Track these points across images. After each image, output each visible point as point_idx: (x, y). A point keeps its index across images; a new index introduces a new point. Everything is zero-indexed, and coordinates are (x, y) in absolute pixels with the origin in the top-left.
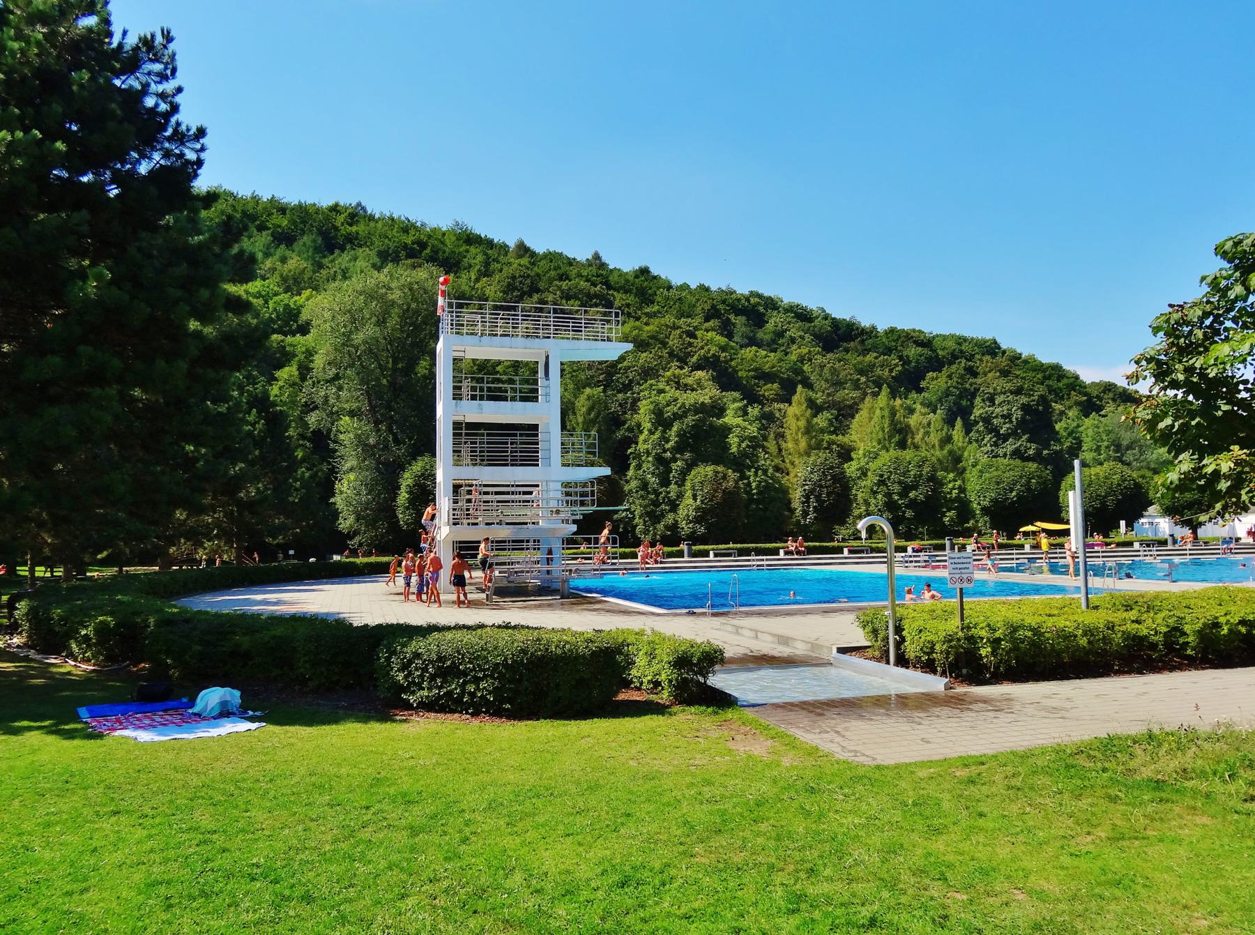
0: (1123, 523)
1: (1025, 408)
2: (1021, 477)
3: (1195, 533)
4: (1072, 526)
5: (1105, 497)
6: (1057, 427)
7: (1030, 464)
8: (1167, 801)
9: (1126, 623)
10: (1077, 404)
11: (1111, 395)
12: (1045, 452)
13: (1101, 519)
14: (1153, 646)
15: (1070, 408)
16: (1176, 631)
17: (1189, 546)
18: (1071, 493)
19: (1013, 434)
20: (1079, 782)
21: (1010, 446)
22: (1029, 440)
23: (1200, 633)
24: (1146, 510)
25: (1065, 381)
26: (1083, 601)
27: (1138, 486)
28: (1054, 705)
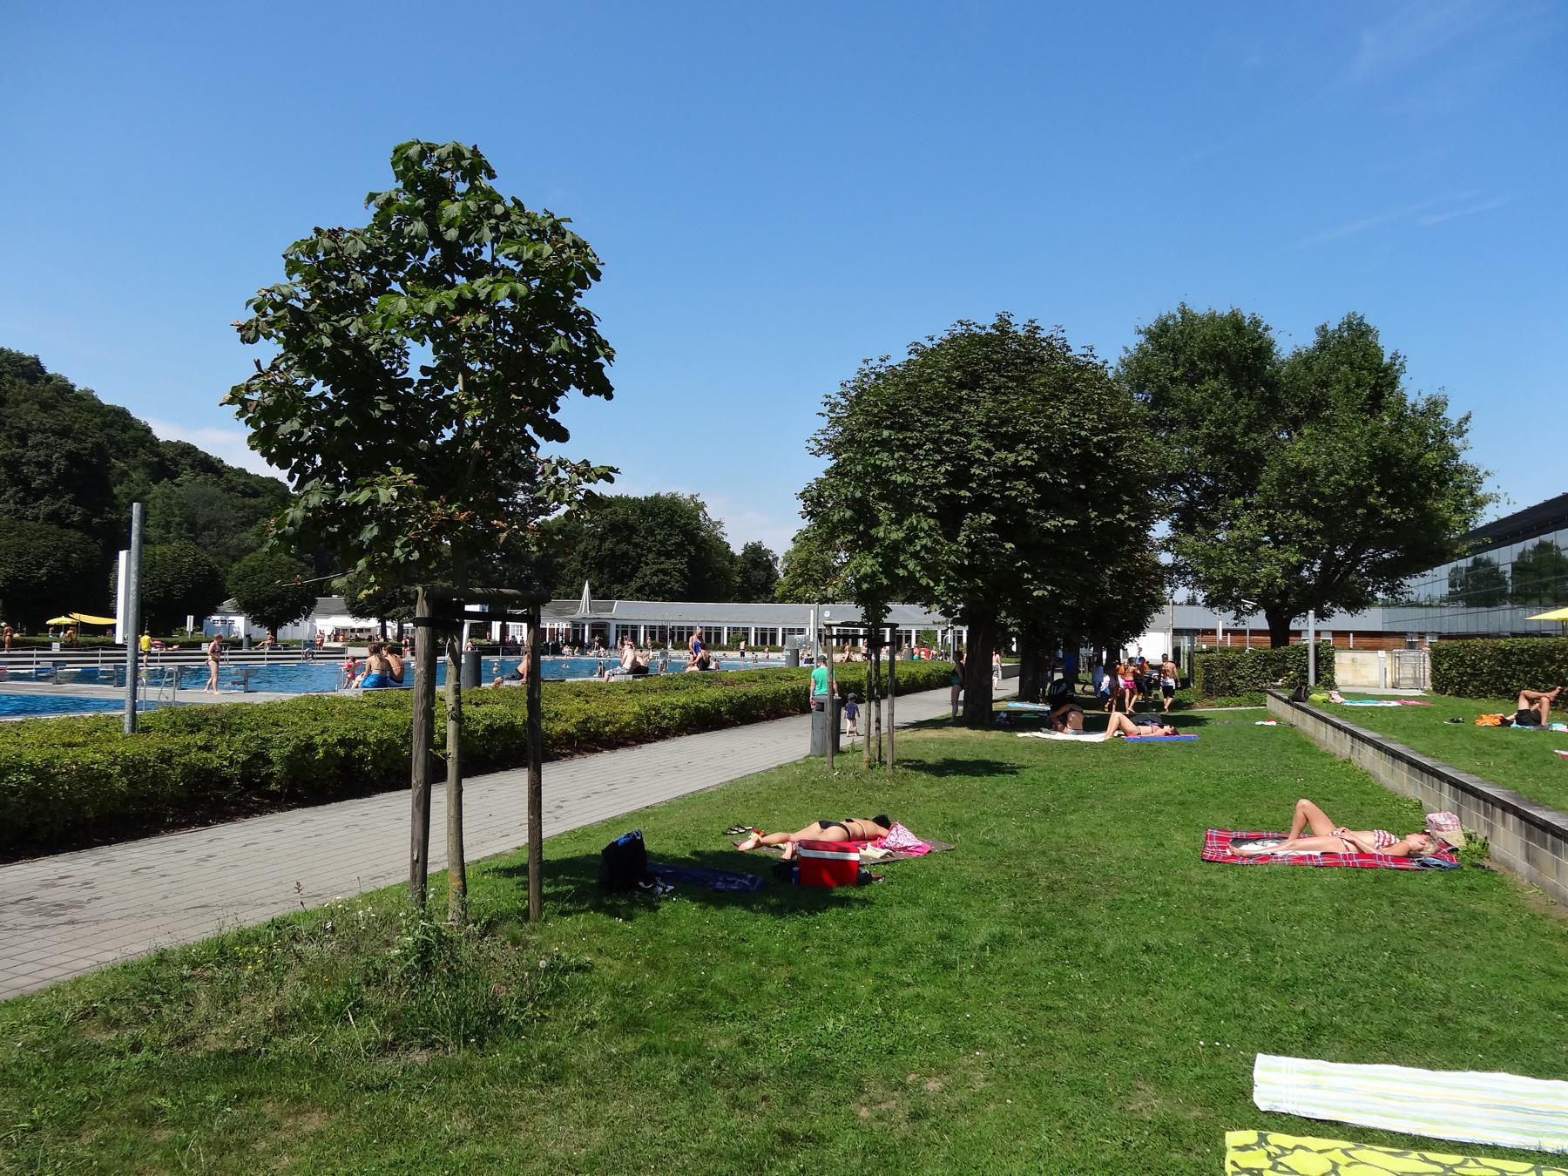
0: (190, 619)
1: (71, 457)
2: (57, 548)
3: (274, 633)
4: (119, 621)
5: (171, 584)
6: (115, 491)
7: (72, 532)
8: (252, 1095)
9: (190, 748)
10: (146, 465)
11: (189, 461)
12: (96, 520)
13: (158, 615)
14: (226, 782)
15: (135, 469)
16: (260, 758)
17: (267, 650)
18: (123, 554)
19: (51, 490)
20: (82, 1090)
21: (44, 506)
22: (73, 502)
23: (289, 760)
24: (220, 604)
25: (132, 433)
26: (127, 720)
27: (213, 573)
28: (59, 898)
